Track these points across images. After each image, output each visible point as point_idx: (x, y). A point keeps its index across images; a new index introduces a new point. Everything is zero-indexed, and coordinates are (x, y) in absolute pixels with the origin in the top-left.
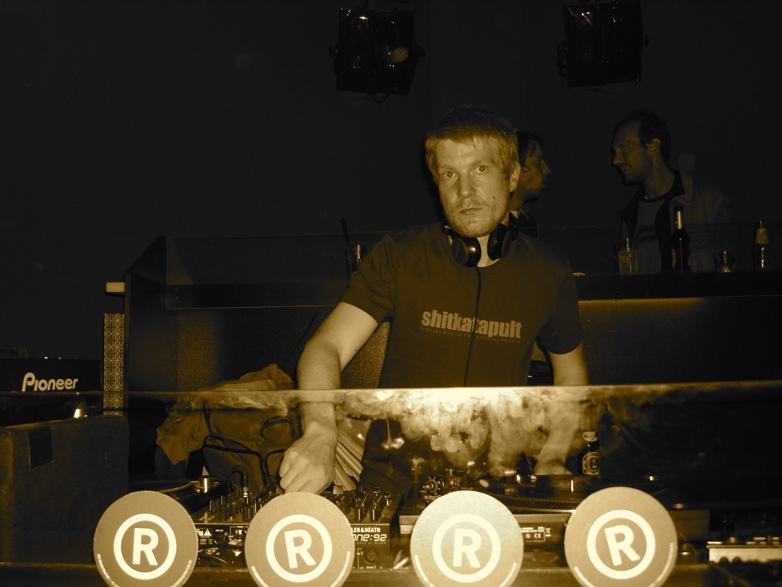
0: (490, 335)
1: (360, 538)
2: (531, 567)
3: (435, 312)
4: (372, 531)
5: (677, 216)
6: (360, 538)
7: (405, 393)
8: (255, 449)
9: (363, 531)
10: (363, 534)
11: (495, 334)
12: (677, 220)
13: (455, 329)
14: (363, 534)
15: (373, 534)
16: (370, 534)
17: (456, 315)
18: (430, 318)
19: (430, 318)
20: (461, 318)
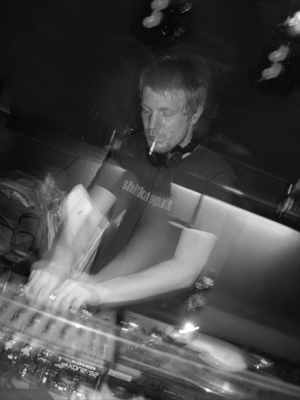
0: (154, 206)
1: (80, 369)
2: (11, 188)
3: (132, 182)
4: (90, 368)
5: (289, 187)
6: (80, 369)
7: (184, 373)
8: (12, 226)
9: (83, 365)
10: (83, 368)
11: (157, 205)
12: (289, 188)
13: (138, 196)
14: (83, 368)
15: (90, 370)
16: (88, 369)
17: (142, 188)
18: (127, 185)
19: (127, 185)
20: (144, 191)
